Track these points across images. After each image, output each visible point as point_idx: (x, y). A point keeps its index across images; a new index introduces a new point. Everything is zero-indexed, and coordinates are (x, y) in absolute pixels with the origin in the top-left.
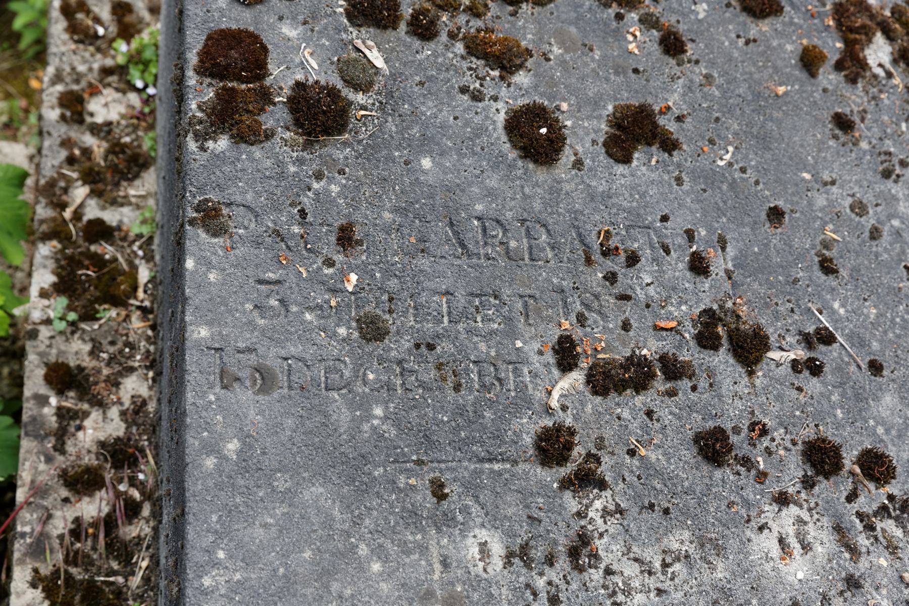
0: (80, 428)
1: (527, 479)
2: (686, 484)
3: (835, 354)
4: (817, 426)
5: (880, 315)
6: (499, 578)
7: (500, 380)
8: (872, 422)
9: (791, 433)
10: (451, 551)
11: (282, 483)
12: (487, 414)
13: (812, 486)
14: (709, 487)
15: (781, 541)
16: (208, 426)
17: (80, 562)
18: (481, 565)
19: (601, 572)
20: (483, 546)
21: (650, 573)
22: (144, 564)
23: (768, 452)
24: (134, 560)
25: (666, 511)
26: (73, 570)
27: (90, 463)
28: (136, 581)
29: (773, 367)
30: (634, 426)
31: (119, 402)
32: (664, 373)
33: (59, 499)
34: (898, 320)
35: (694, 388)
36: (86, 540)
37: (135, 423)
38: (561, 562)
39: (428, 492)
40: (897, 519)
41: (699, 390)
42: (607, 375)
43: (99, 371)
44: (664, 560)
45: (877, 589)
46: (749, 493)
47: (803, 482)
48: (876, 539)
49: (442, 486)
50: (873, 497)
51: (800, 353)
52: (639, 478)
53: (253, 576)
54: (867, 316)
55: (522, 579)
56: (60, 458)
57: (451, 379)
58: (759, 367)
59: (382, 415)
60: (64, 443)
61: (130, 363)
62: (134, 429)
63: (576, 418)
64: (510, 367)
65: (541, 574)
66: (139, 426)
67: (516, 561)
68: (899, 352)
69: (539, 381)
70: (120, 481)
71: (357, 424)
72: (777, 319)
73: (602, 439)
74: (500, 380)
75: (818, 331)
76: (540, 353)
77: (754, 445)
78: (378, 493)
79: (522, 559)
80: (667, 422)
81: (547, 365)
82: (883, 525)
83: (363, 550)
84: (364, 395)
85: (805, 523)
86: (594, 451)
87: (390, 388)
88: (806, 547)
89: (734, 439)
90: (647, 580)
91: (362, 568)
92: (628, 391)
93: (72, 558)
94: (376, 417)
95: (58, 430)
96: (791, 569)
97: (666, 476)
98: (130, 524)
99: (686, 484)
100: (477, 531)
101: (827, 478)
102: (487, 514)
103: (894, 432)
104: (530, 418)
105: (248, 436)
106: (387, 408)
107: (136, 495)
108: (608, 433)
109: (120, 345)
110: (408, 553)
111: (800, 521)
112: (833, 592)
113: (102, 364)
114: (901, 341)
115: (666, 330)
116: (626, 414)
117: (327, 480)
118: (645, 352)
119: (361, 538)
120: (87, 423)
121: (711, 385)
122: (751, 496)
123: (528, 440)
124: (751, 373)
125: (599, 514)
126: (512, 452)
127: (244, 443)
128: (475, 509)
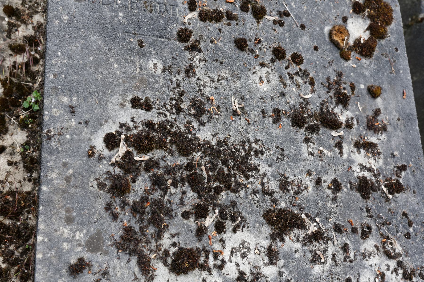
0: (17, 30)
1: (173, 45)
2: (230, 55)
3: (289, 20)
4: (279, 43)
5: (307, 10)
6: (160, 75)
7: (167, 10)
8: (298, 45)
9: (269, 44)
10: (144, 64)
11: (83, 33)
12: (161, 21)
13: (274, 62)
14: (238, 57)
15: (260, 78)
16: (57, 10)
17: (15, 76)
18: (154, 70)
19: (196, 79)
20: (155, 65)
21: (213, 82)
22: (40, 80)
23: (260, 49)
24: (36, 78)
25: (221, 63)
26: (13, 79)
27: (20, 43)
28: (36, 85)
29: (266, 21)
30: (214, 33)
31: (32, 23)
32: (227, 17)
33: (8, 54)
34: (314, 12)
35: (237, 24)
36: (18, 69)
37: (38, 31)
38: (182, 74)
39: (137, 44)
40: (301, 77)
41: (239, 25)
42: (206, 14)
43: (25, 11)
44: (218, 78)
45: (291, 97)
46: (251, 61)
47: (271, 60)
48: (293, 82)
49: (142, 42)
50: (294, 69)
51: (277, 18)
52: (213, 51)
53: (71, 62)
54: (303, 9)
55: (167, 77)
56: (9, 40)
57: (149, 8)
58: (261, 20)
59: (122, 16)
60: (10, 35)
61: (37, 10)
62: (38, 33)
63: (193, 27)
64: (171, 7)
65: (175, 77)
66: (39, 32)
67: (166, 71)
68: (312, 23)
69: (181, 13)
70: (32, 51)
71: (112, 18)
72: (271, 5)
73: (202, 36)
74: (167, 10)
75: (284, 11)
76: (183, 4)
77: (256, 46)
78: (118, 42)
79: (168, 70)
80: (226, 34)
81: (185, 8)
82: (296, 78)
83: (112, 60)
84: (116, 8)
85: (270, 74)
86: (198, 39)
87: (127, 8)
88: (269, 81)
89: (249, 43)
90: (212, 84)
91: (111, 65)
92: (213, 21)
93: (12, 74)
94: (120, 16)
95: (8, 30)
96: (262, 87)
97: (223, 52)
98: (35, 66)
99: (230, 55)
100: (153, 59)
101: (279, 60)
102: (157, 54)
103: (305, 49)
104: (177, 25)
105: (71, 15)
106: (124, 14)
107: (38, 56)
108: (204, 34)
109: (33, 3)
110: (128, 63)
111: (268, 73)
112: (275, 96)
113: (26, 9)
114: (313, 20)
115: (230, 3)
116: (211, 29)
117: (100, 35)
118: (221, 9)
119: (111, 56)
120: (20, 29)
121: (243, 24)
122: (252, 62)
123: (175, 32)
124: (258, 22)
125: (198, 60)
126: (169, 35)
127: (70, 18)
128: (153, 52)
